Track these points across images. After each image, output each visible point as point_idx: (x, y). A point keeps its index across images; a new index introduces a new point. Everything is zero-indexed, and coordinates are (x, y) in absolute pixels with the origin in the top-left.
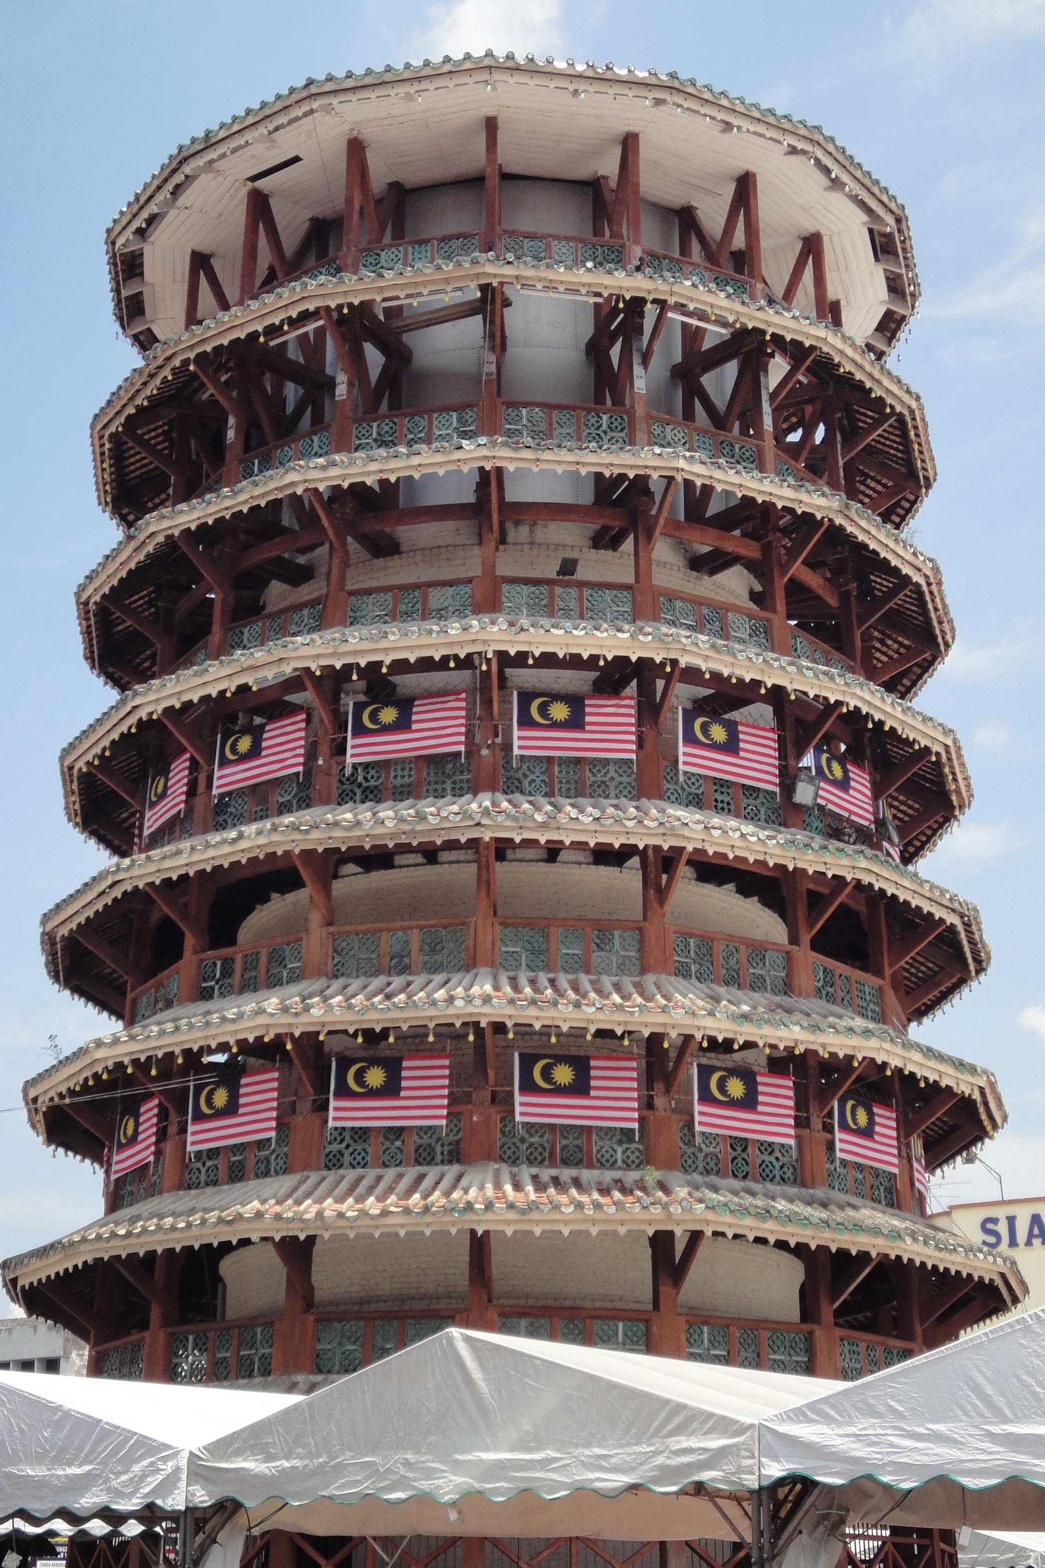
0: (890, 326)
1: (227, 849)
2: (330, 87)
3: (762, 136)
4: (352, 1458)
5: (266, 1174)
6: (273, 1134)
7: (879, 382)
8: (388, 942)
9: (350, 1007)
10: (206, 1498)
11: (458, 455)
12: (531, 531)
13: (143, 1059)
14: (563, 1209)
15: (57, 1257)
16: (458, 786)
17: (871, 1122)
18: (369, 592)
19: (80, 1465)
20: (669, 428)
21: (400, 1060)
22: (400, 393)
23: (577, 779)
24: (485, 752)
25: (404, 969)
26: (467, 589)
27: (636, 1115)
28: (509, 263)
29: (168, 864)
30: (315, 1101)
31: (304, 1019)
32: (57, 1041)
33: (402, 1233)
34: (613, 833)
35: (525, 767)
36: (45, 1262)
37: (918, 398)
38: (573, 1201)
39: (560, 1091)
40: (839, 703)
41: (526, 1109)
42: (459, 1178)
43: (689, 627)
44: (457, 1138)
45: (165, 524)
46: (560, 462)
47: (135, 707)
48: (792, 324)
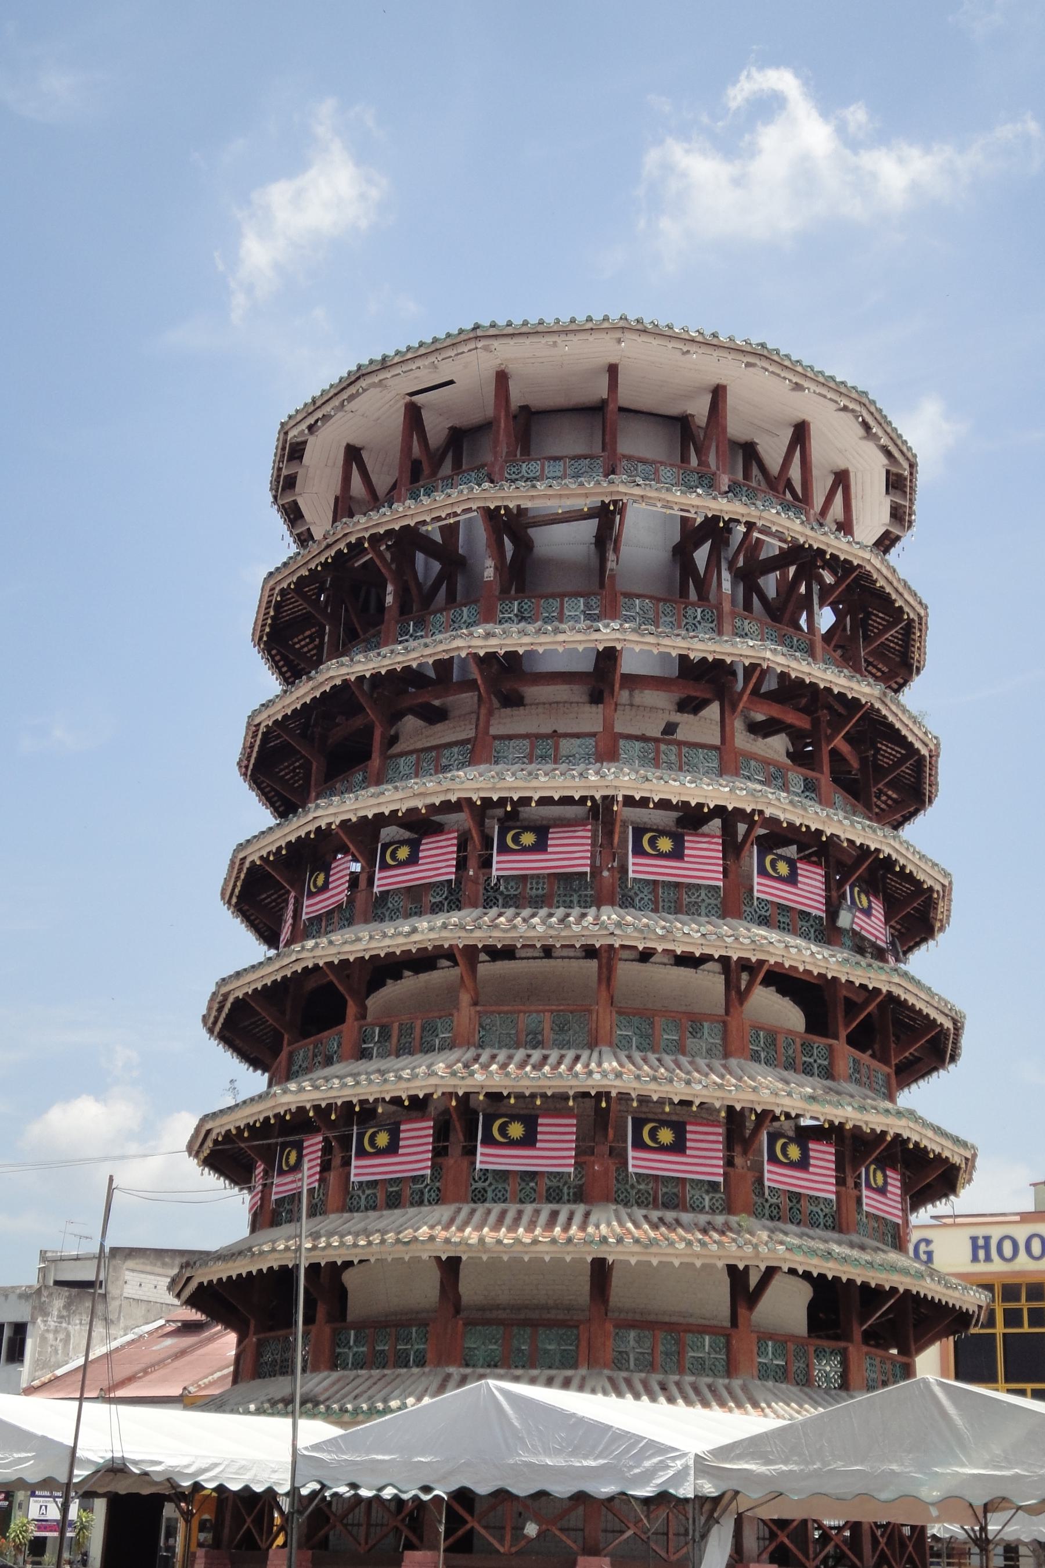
0: (886, 543)
1: (401, 940)
2: (492, 332)
3: (825, 397)
4: (844, 1466)
5: (421, 1203)
6: (429, 1172)
7: (901, 595)
8: (527, 1021)
9: (508, 1074)
10: (712, 1490)
11: (596, 636)
12: (631, 695)
13: (323, 1106)
14: (677, 1245)
15: (243, 1262)
16: (583, 899)
17: (886, 1183)
18: (510, 737)
19: (595, 1459)
20: (746, 622)
21: (537, 1117)
22: (524, 576)
23: (676, 899)
24: (606, 874)
25: (537, 1043)
26: (591, 741)
27: (721, 1171)
28: (638, 485)
29: (347, 948)
30: (464, 1147)
31: (469, 1082)
32: (236, 1084)
33: (547, 1258)
34: (714, 946)
35: (636, 888)
36: (230, 1264)
37: (926, 608)
38: (682, 1239)
39: (663, 1149)
40: (877, 850)
41: (637, 1162)
42: (587, 1215)
43: (761, 782)
44: (580, 1182)
45: (344, 670)
46: (674, 647)
47: (315, 818)
48: (846, 547)
